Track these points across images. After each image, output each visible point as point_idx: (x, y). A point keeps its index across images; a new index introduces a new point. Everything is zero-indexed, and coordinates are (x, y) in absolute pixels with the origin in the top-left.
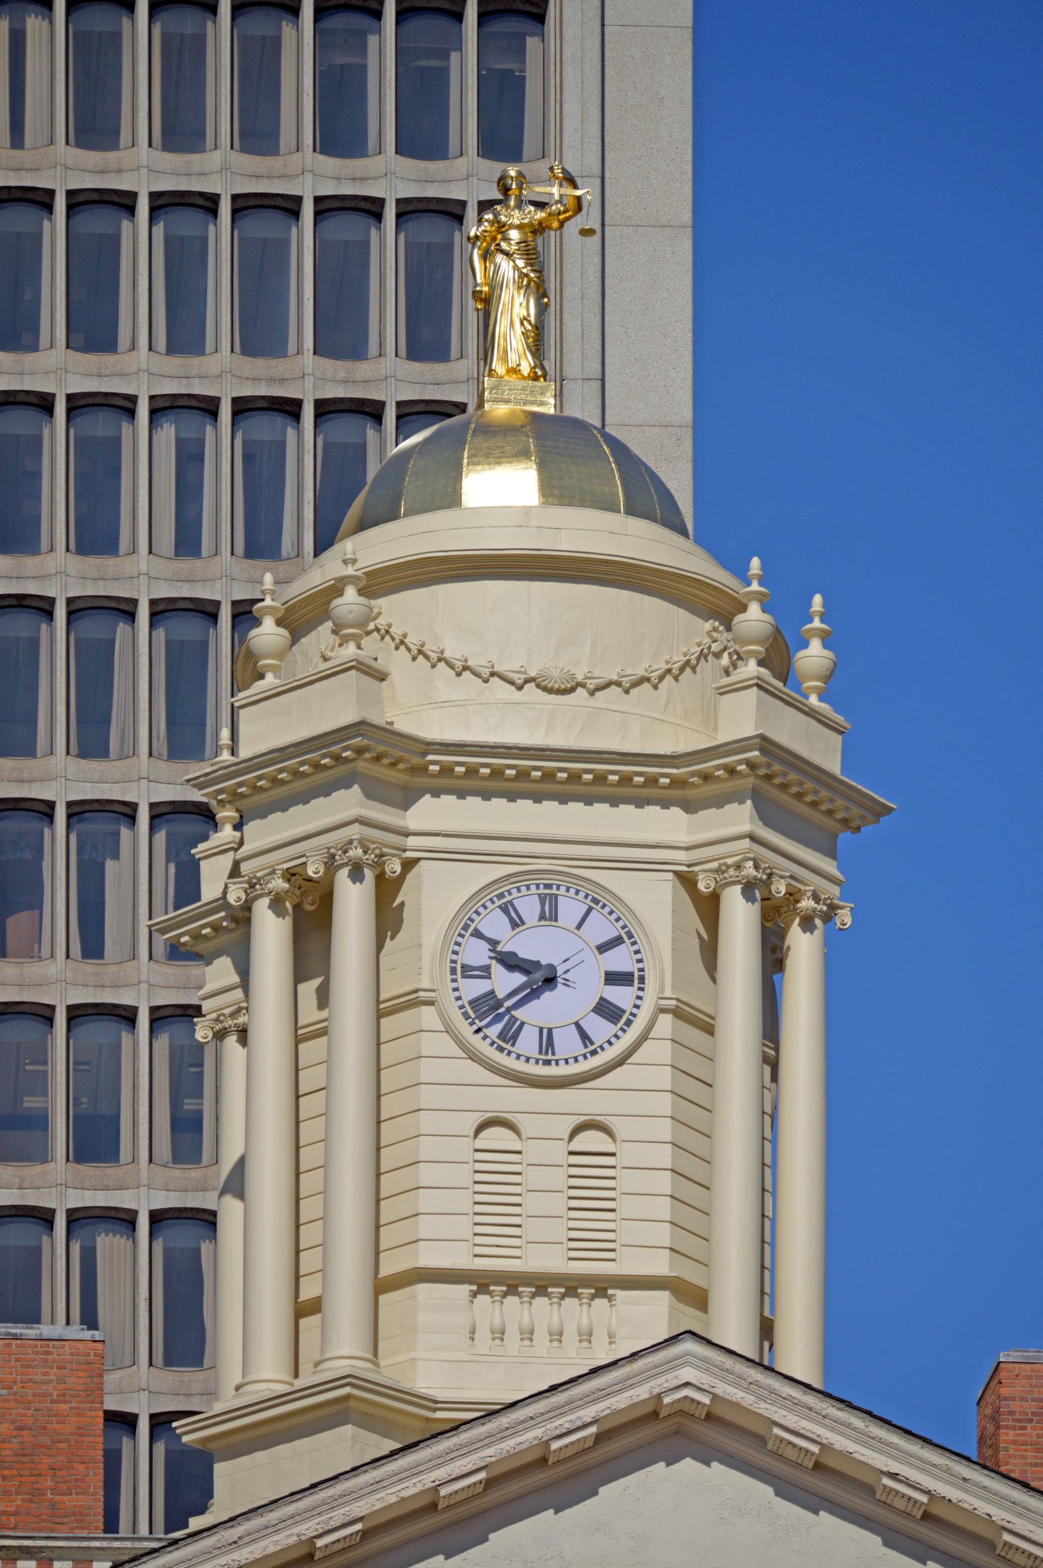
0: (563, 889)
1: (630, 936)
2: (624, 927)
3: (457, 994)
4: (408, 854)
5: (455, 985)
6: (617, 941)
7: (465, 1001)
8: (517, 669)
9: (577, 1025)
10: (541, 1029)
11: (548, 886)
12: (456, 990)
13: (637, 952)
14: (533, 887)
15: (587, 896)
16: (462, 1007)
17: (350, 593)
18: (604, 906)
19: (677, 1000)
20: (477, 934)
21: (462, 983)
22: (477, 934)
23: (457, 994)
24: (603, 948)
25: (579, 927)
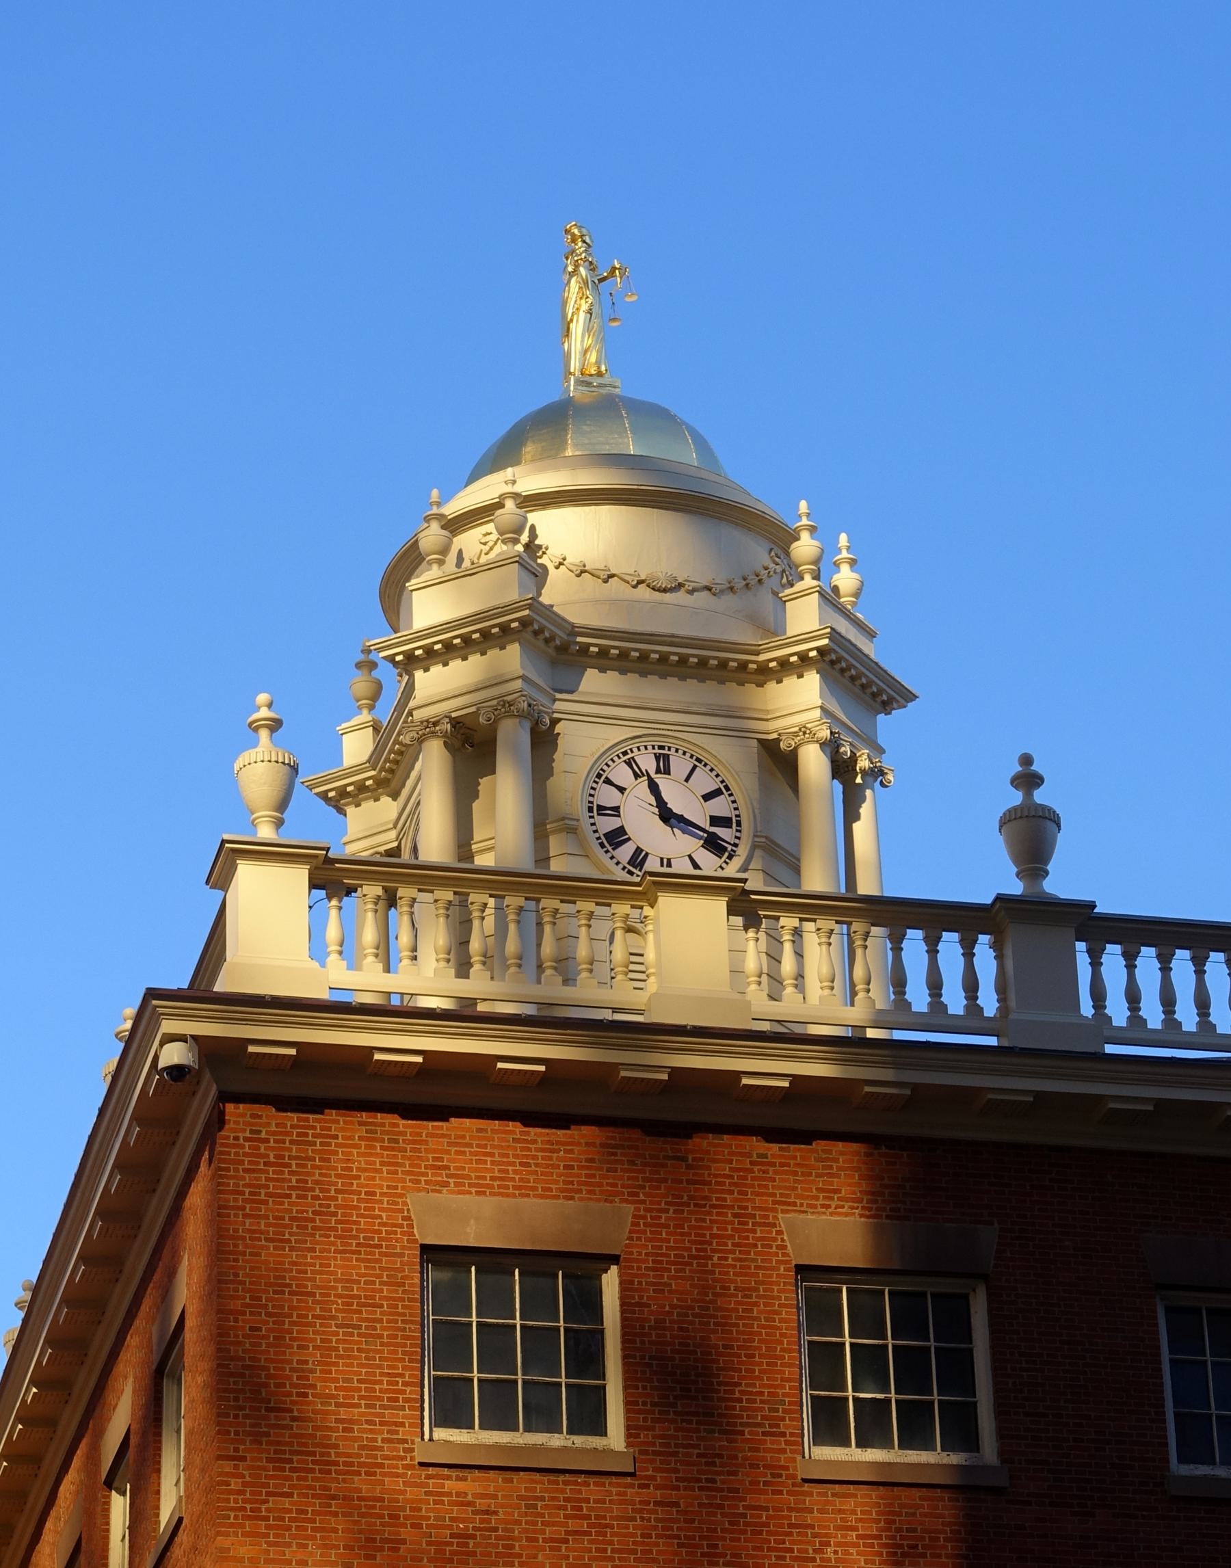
0: (673, 750)
1: (727, 788)
2: (722, 782)
3: (594, 828)
4: (556, 715)
5: (592, 821)
6: (717, 793)
7: (601, 833)
8: (632, 572)
9: (690, 856)
10: (662, 859)
11: (661, 747)
12: (593, 824)
13: (734, 802)
14: (650, 748)
15: (692, 756)
16: (599, 838)
17: (510, 504)
18: (705, 765)
19: (766, 838)
20: (608, 781)
21: (598, 819)
22: (608, 781)
23: (594, 828)
24: (707, 797)
25: (687, 780)
